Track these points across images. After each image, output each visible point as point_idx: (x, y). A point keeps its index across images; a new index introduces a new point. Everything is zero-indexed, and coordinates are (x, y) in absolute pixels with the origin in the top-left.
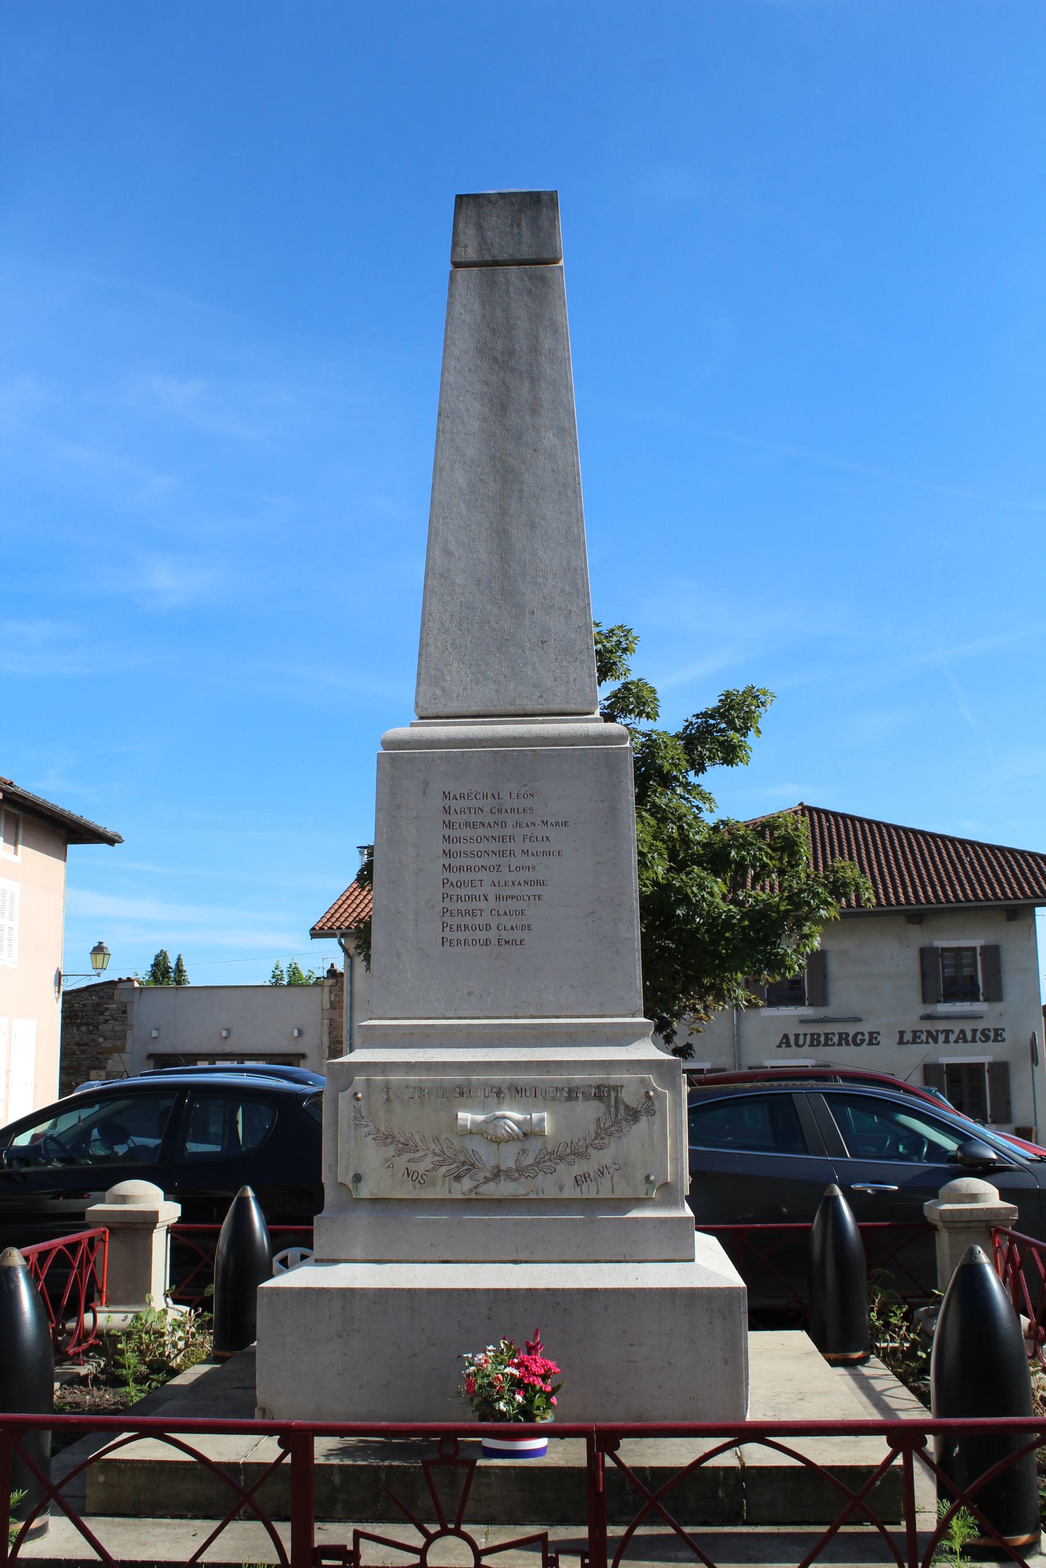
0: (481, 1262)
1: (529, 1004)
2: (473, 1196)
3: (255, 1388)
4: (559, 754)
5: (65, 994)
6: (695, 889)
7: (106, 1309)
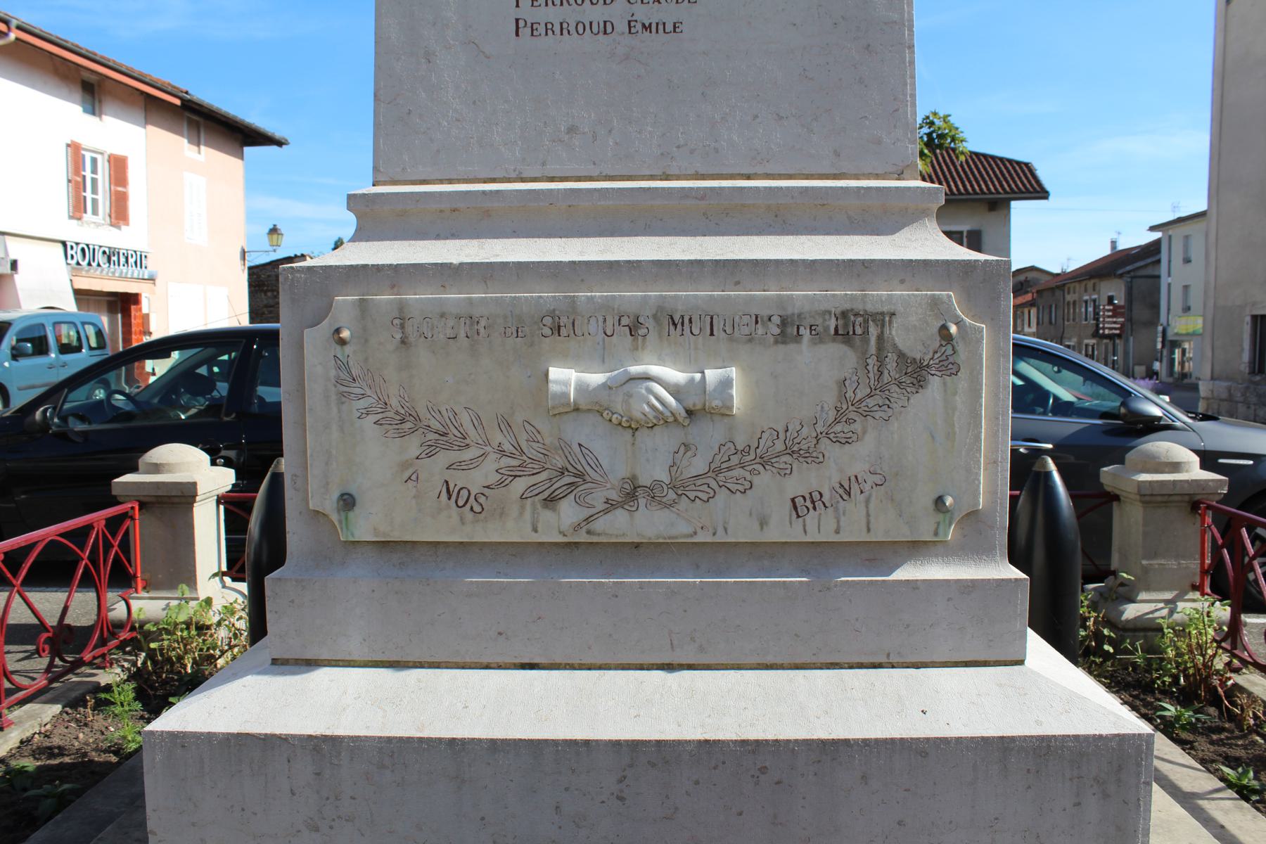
0: (600, 668)
1: (692, 152)
2: (582, 537)
5: (250, 268)
7: (146, 595)
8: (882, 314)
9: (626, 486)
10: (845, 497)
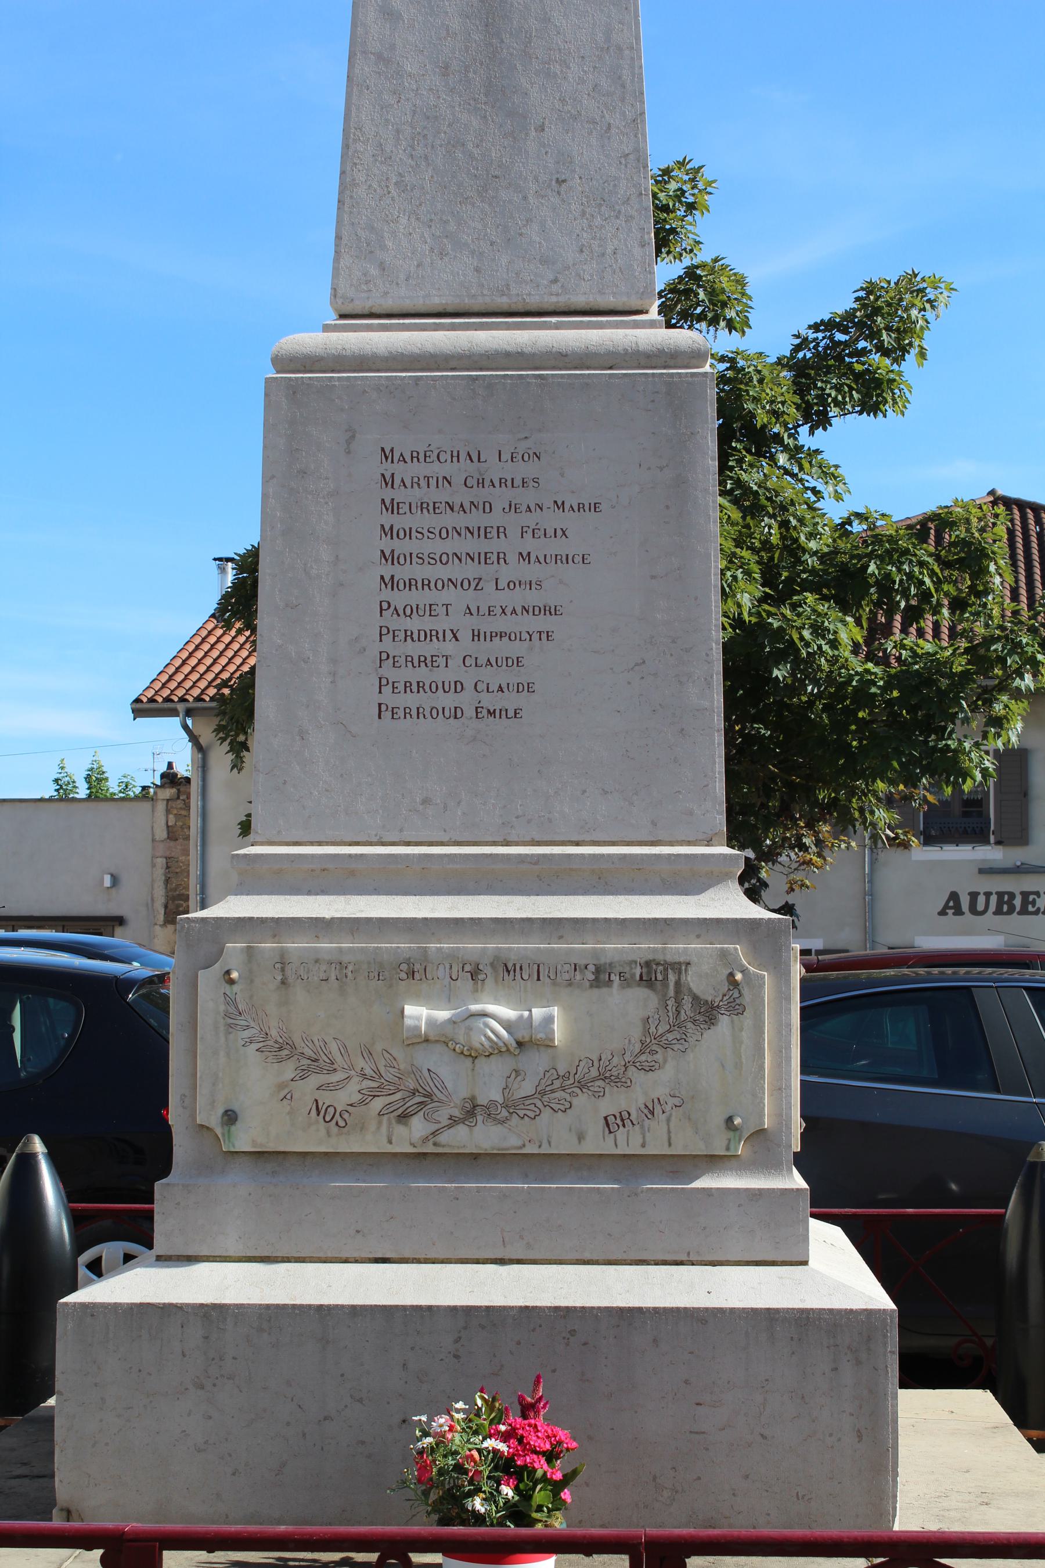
0: (442, 1262)
2: (429, 1149)
3: (53, 1476)
4: (586, 384)
6: (806, 634)
8: (680, 963)
9: (467, 1105)
10: (650, 1116)
